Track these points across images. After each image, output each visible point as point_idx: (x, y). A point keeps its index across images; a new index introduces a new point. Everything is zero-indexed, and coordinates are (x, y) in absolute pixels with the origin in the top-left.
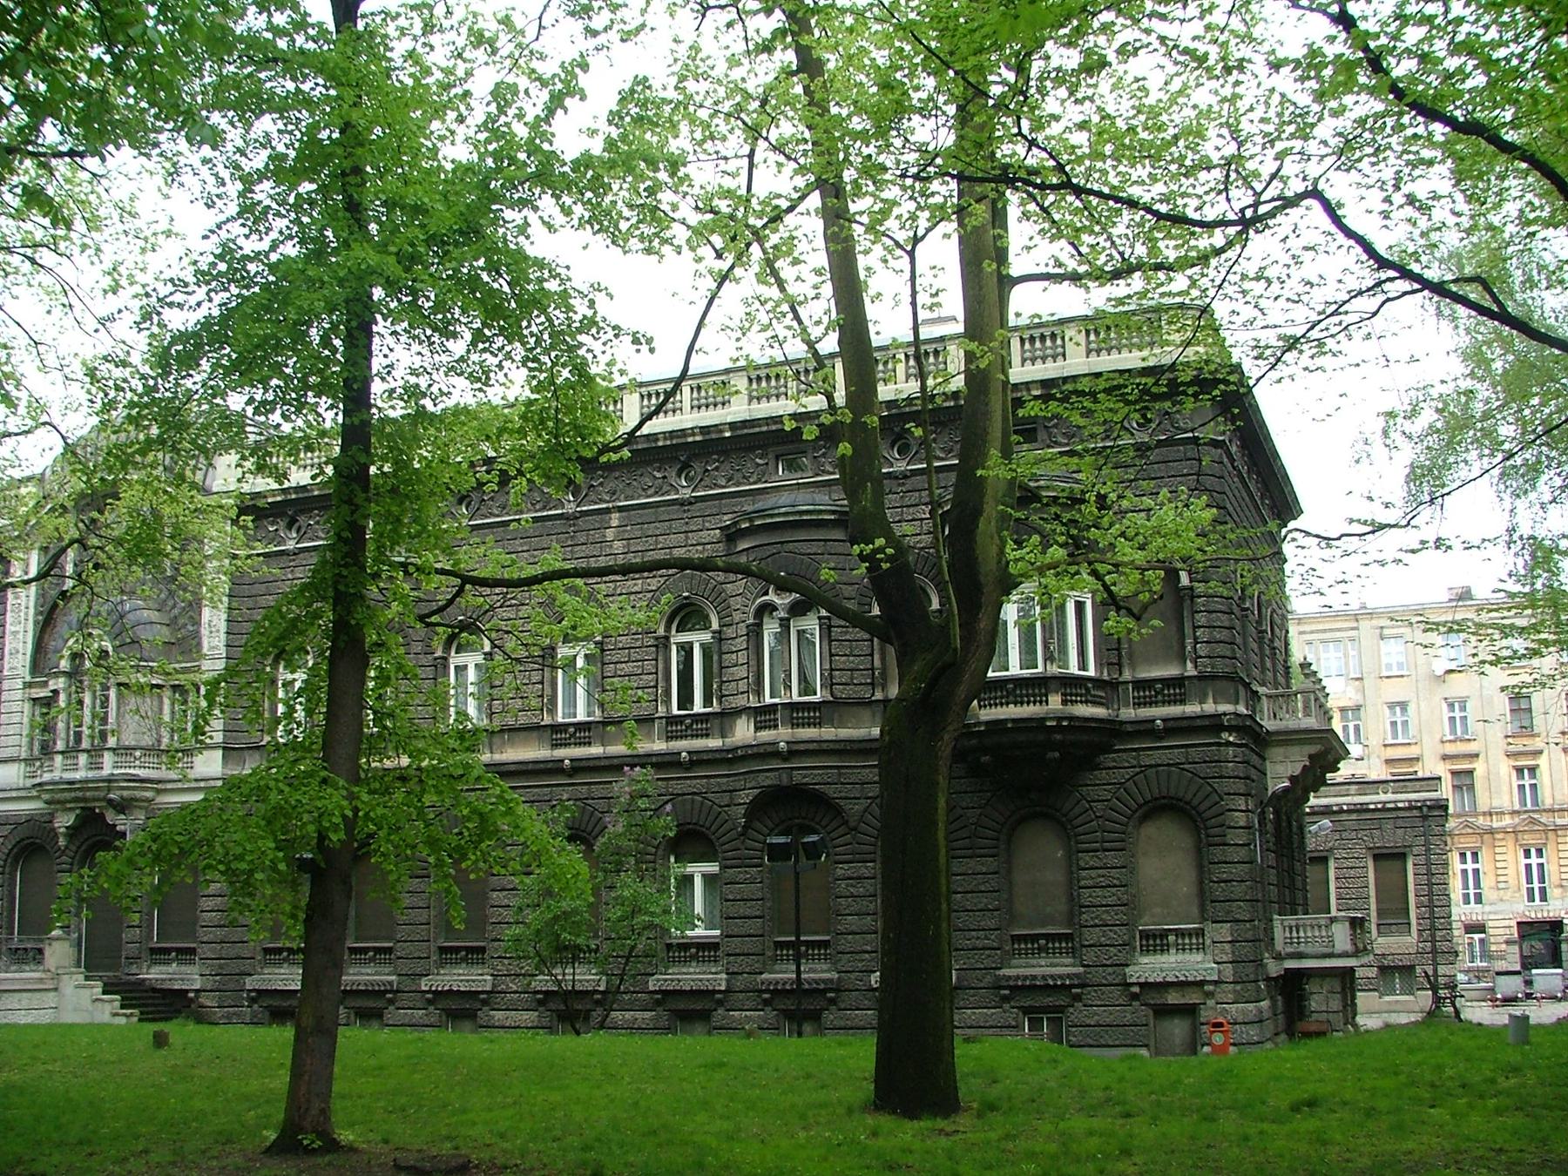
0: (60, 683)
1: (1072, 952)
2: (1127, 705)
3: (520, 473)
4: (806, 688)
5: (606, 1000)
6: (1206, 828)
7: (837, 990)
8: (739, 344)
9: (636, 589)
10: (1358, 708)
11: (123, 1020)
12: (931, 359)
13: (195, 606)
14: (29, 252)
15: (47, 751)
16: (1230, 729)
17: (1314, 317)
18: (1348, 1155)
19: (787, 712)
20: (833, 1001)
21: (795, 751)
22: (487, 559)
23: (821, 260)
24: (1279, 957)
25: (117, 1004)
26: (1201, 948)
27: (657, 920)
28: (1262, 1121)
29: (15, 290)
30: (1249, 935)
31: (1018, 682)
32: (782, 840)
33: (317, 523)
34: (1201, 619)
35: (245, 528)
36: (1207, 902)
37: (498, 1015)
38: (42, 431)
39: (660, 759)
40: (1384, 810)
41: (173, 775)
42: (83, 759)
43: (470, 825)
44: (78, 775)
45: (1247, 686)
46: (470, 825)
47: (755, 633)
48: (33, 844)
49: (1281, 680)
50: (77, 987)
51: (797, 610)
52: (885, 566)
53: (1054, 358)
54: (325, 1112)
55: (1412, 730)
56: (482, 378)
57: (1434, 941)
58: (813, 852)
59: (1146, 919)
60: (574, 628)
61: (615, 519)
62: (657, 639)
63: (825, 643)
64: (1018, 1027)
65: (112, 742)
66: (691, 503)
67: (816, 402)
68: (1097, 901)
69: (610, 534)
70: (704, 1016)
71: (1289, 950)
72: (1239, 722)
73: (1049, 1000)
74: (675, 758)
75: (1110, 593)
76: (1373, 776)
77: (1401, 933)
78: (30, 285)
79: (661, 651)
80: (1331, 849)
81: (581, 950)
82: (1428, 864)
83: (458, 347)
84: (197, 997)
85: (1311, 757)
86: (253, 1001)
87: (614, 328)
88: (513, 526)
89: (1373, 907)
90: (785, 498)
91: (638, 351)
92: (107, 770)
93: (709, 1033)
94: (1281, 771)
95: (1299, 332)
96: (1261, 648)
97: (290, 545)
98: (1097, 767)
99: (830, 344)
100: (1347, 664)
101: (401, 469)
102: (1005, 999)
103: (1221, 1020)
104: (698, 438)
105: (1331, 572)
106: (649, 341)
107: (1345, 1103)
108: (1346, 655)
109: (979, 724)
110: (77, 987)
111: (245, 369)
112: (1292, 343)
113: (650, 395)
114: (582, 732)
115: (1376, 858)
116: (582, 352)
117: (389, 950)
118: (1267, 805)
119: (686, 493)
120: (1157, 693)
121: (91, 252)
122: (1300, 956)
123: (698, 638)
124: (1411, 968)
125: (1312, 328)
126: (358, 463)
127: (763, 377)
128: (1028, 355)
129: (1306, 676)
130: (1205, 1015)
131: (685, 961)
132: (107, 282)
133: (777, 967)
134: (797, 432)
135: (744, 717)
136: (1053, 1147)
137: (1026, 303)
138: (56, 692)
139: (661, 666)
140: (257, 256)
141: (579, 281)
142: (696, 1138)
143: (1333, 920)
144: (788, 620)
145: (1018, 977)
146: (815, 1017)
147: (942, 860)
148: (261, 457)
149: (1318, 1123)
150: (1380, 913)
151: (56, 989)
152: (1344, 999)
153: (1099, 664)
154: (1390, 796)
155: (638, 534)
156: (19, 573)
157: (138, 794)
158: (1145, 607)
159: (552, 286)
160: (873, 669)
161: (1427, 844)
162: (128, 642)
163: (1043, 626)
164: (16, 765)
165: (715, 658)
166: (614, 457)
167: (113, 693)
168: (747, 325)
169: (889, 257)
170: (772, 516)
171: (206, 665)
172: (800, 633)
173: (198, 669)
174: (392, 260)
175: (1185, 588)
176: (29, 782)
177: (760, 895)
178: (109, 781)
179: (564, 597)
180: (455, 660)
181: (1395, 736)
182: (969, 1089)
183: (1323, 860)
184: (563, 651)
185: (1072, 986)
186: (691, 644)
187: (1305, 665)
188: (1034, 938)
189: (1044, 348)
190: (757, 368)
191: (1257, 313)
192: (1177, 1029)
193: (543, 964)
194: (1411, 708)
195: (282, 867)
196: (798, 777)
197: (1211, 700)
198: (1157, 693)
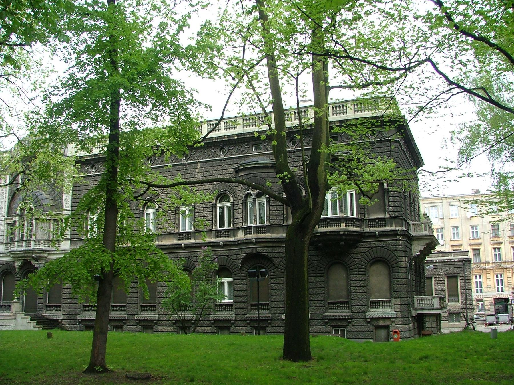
0: (17, 218)
2: (366, 227)
3: (168, 150)
4: (262, 221)
5: (196, 323)
6: (392, 267)
8: (240, 108)
10: (442, 228)
11: (37, 329)
12: (303, 114)
13: (61, 193)
15: (12, 241)
20: (270, 324)
21: (258, 242)
22: (157, 178)
24: (416, 310)
25: (35, 324)
26: (390, 306)
27: (212, 297)
30: (406, 302)
34: (391, 199)
35: (77, 168)
36: (392, 292)
37: (160, 328)
39: (213, 244)
40: (448, 262)
41: (54, 249)
42: (24, 243)
43: (151, 265)
44: (22, 249)
46: (151, 265)
47: (245, 203)
49: (417, 219)
51: (259, 195)
52: (287, 181)
53: (343, 113)
55: (460, 236)
56: (155, 119)
57: (466, 305)
59: (372, 297)
60: (185, 201)
61: (199, 165)
63: (268, 207)
64: (330, 332)
66: (224, 160)
67: (265, 127)
69: (197, 170)
70: (227, 328)
71: (419, 307)
73: (340, 324)
74: (218, 244)
76: (447, 251)
77: (456, 302)
78: (7, 88)
80: (433, 275)
81: (187, 306)
83: (148, 109)
84: (61, 321)
85: (427, 244)
86: (80, 323)
87: (199, 103)
88: (166, 167)
89: (447, 293)
90: (255, 159)
93: (229, 334)
94: (417, 249)
95: (424, 105)
97: (92, 174)
98: (357, 247)
99: (270, 108)
100: (439, 214)
101: (129, 149)
102: (326, 323)
104: (226, 139)
105: (433, 184)
106: (210, 107)
107: (437, 357)
108: (438, 212)
109: (318, 233)
111: (78, 116)
112: (421, 109)
113: (210, 125)
114: (188, 235)
115: (448, 277)
116: (188, 111)
117: (124, 306)
119: (222, 157)
121: (27, 77)
122: (423, 309)
123: (226, 205)
127: (248, 119)
128: (335, 112)
129: (425, 218)
130: (392, 328)
131: (222, 310)
132: (32, 87)
133: (252, 312)
134: (259, 137)
137: (334, 95)
138: (15, 221)
139: (214, 214)
140: (81, 79)
141: (188, 87)
143: (433, 298)
144: (256, 199)
145: (330, 316)
146: (264, 328)
147: (306, 277)
148: (83, 145)
151: (15, 319)
152: (437, 323)
153: (357, 214)
154: (452, 257)
155: (207, 170)
157: (42, 255)
158: (373, 195)
159: (179, 89)
160: (283, 215)
161: (464, 273)
162: (39, 205)
163: (339, 201)
166: (199, 145)
168: (243, 102)
169: (289, 80)
172: (260, 203)
173: (62, 214)
174: (126, 80)
175: (386, 189)
177: (246, 289)
178: (33, 251)
179: (182, 191)
180: (146, 211)
181: (454, 238)
182: (314, 352)
184: (182, 209)
185: (348, 319)
186: (224, 207)
188: (336, 303)
189: (340, 110)
191: (410, 99)
192: (383, 333)
193: (175, 311)
194: (460, 229)
195: (90, 278)
196: (259, 250)
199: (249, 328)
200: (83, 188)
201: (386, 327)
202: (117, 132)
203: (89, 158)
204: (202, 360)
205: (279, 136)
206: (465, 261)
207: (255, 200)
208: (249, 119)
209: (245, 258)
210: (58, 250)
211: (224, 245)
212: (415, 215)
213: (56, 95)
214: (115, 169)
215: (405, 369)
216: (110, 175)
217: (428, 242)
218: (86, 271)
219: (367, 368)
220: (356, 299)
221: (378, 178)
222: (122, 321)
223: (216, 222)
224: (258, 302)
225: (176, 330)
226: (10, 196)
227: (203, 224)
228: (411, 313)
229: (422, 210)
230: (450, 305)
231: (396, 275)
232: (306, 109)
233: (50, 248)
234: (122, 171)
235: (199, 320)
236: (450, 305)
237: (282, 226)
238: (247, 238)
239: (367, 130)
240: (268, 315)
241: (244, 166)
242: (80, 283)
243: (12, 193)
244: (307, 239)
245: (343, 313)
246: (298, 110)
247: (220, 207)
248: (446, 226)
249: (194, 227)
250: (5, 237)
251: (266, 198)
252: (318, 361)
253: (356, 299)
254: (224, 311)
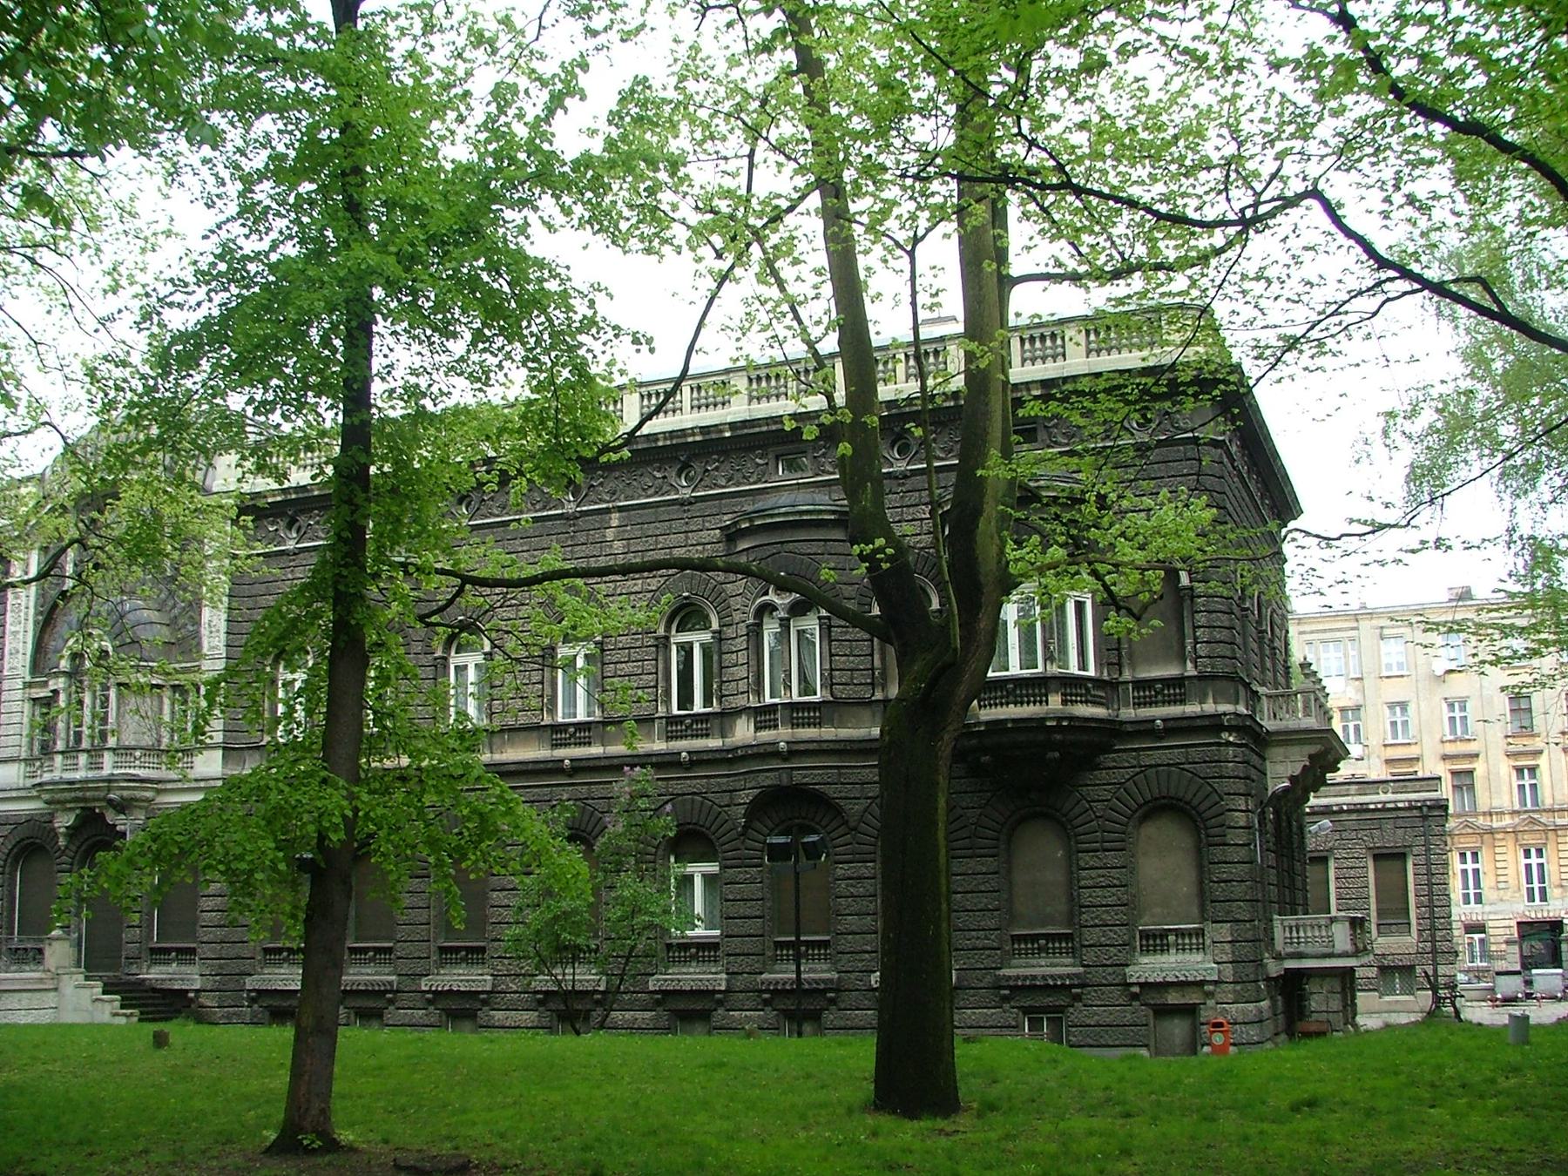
0: (60, 683)
1: (1072, 952)
2: (1127, 705)
3: (520, 473)
4: (806, 688)
5: (606, 1000)
6: (1206, 828)
7: (837, 990)
8: (739, 344)
9: (636, 589)
10: (1358, 708)
11: (123, 1020)
13: (195, 606)
14: (29, 252)
15: (47, 751)
16: (1230, 729)
17: (1314, 317)
19: (787, 712)
20: (833, 1001)
21: (795, 751)
22: (487, 559)
23: (821, 260)
24: (1279, 957)
25: (117, 1004)
26: (1201, 948)
27: (657, 920)
28: (1262, 1121)
29: (15, 290)
30: (1249, 935)
31: (1018, 682)
32: (782, 840)
33: (317, 523)
34: (1201, 619)
35: (245, 528)
36: (1207, 902)
37: (498, 1015)
38: (42, 431)
39: (660, 759)
40: (1384, 810)
41: (173, 775)
42: (83, 759)
43: (470, 825)
44: (78, 775)
45: (1247, 686)
46: (470, 825)
47: (755, 633)
48: (33, 844)
49: (1281, 680)
50: (77, 987)
51: (797, 610)
52: (885, 566)
53: (1054, 358)
54: (325, 1112)
55: (1412, 730)
56: (482, 378)
57: (1434, 941)
58: (813, 852)
59: (1146, 919)
60: (574, 628)
61: (615, 519)
62: (657, 639)
63: (825, 643)
64: (1018, 1027)
65: (112, 742)
66: (691, 503)
67: (816, 402)
68: (1097, 901)
69: (610, 534)
70: (704, 1016)
71: (1289, 950)
72: (1239, 722)
73: (1049, 1000)
74: (675, 758)
75: (1110, 593)
76: (1373, 776)
77: (1401, 933)
78: (30, 285)
79: (661, 651)
80: (1331, 849)
81: (581, 950)
82: (1428, 864)
83: (458, 347)
84: (197, 997)
85: (1311, 757)
86: (253, 1001)
87: (614, 328)
88: (513, 526)
89: (1373, 907)
90: (785, 498)
91: (638, 351)
92: (107, 770)
93: (709, 1033)
94: (1281, 771)
95: (1299, 332)
96: (1261, 648)
97: (290, 545)
98: (1097, 767)
99: (830, 344)
100: (1347, 664)
101: (401, 469)
102: (1005, 999)
103: (1221, 1020)
104: (698, 438)
105: (1331, 572)
106: (649, 341)
108: (1346, 655)
109: (979, 724)
110: (77, 987)
111: (245, 369)
112: (1292, 343)
113: (650, 395)
114: (582, 732)
115: (1376, 858)
116: (582, 352)
117: (389, 950)
118: (1267, 805)
119: (686, 493)
120: (1157, 693)
121: (91, 252)
122: (1300, 956)
123: (698, 638)
124: (1411, 968)
125: (1312, 328)
126: (358, 463)
127: (763, 377)
128: (1028, 355)
129: (1306, 676)
130: (1205, 1015)
131: (685, 961)
132: (107, 282)
133: (777, 967)
134: (797, 432)
135: (744, 717)
136: (1053, 1147)
137: (1026, 303)
138: (56, 692)
139: (661, 666)
140: (257, 256)
141: (579, 281)
142: (696, 1138)
143: (1333, 920)
144: (788, 620)
145: (1018, 977)
146: (815, 1017)
147: (942, 860)
148: (261, 457)
150: (1380, 913)
151: (56, 989)
152: (1344, 999)
153: (1099, 664)
154: (1390, 796)
155: (638, 534)
156: (19, 573)
157: (138, 794)
158: (1145, 607)
159: (552, 286)
160: (873, 669)
161: (1427, 844)
162: (128, 642)
163: (1043, 626)
164: (16, 765)
165: (715, 658)
167: (113, 693)
168: (747, 325)
169: (889, 257)
170: (772, 516)
171: (206, 665)
172: (800, 633)
173: (198, 669)
174: (392, 260)
175: (1185, 588)
176: (29, 782)
177: (760, 895)
178: (109, 781)
179: (564, 597)
180: (455, 660)
181: (1395, 736)
182: (969, 1089)
183: (1323, 860)
184: (563, 651)
185: (1072, 986)
186: (691, 644)
187: (1305, 665)
188: (1034, 938)
189: (1044, 348)
190: (757, 368)
191: (1257, 313)
192: (1177, 1029)
193: (543, 964)
194: (1411, 708)
195: (282, 867)
196: (798, 777)
197: (1211, 700)
198: (1157, 693)
239: (1126, 410)
249: (491, 715)
250: (25, 741)
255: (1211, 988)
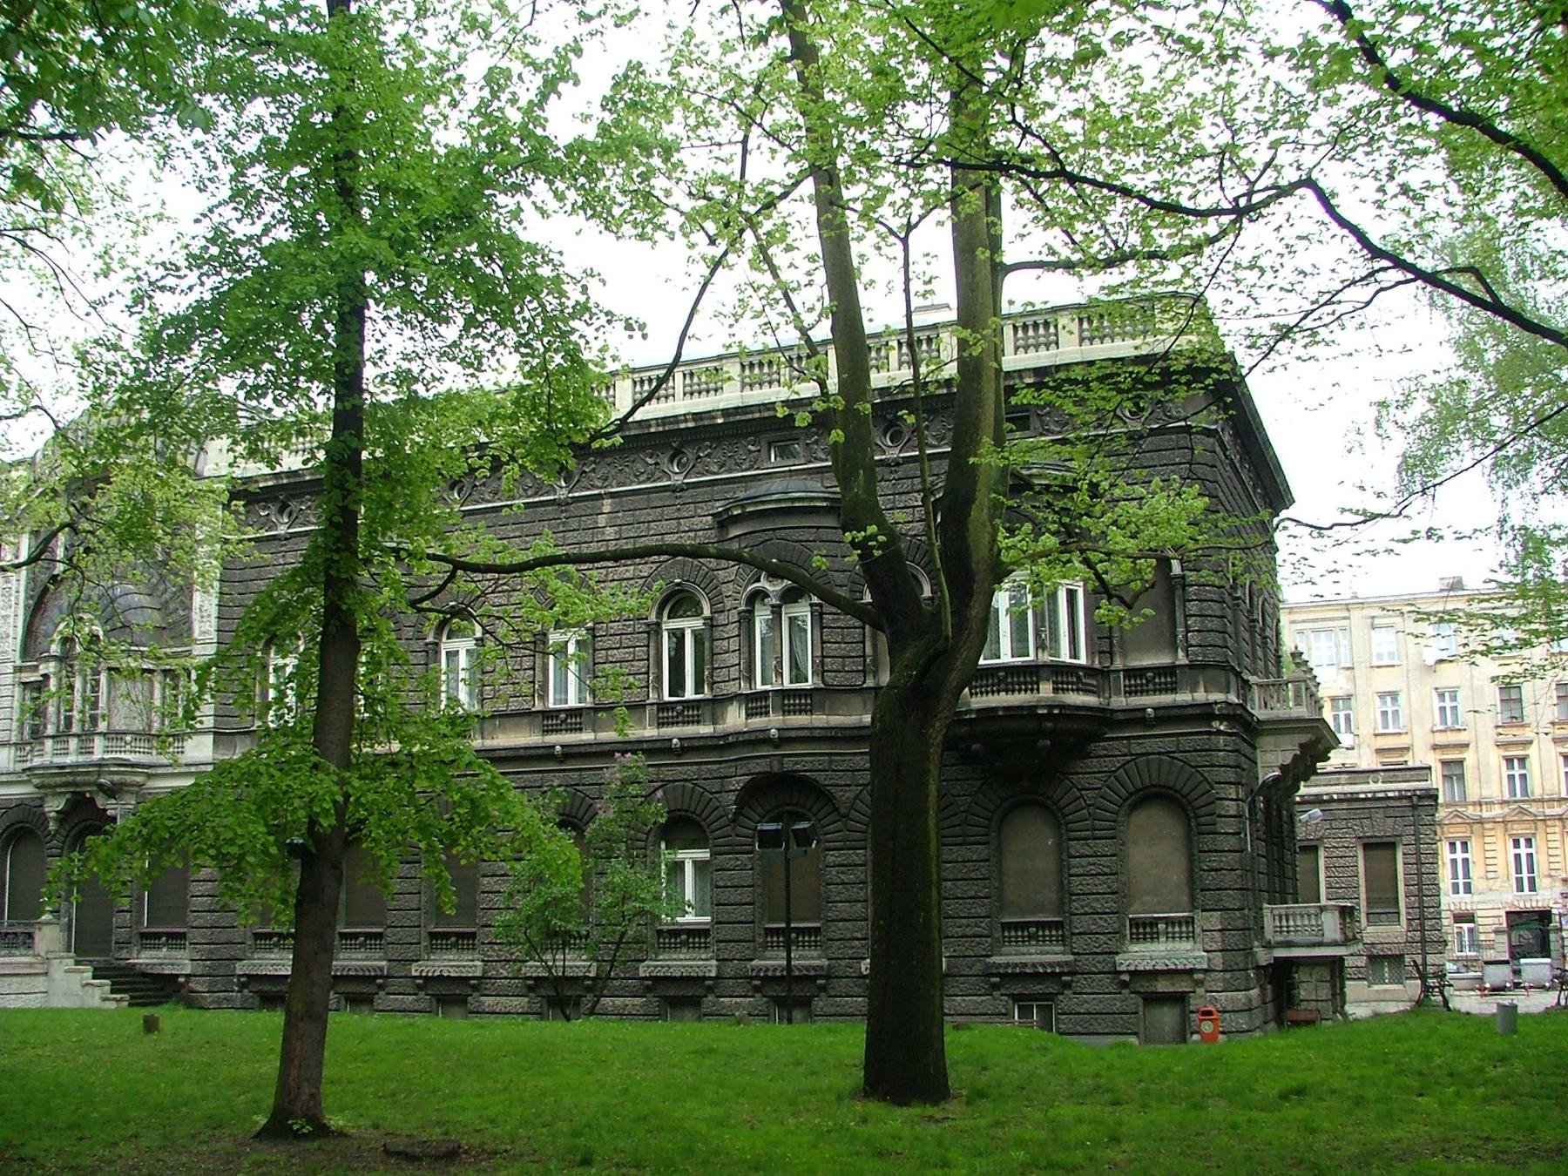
0: (50, 667)
2: (1118, 694)
3: (513, 459)
4: (798, 676)
5: (597, 986)
6: (1197, 817)
8: (732, 331)
10: (1349, 698)
11: (113, 1005)
13: (186, 591)
15: (37, 735)
18: (1336, 1143)
20: (823, 988)
21: (786, 738)
22: (478, 544)
24: (1268, 946)
25: (108, 988)
26: (1191, 936)
27: (647, 907)
30: (1239, 924)
34: (1193, 607)
35: (236, 513)
36: (1197, 890)
37: (489, 1001)
38: (33, 414)
39: (651, 745)
40: (1366, 799)
41: (163, 760)
42: (73, 743)
43: (461, 811)
44: (69, 760)
46: (461, 811)
47: (747, 619)
49: (1272, 669)
51: (789, 597)
52: (877, 553)
53: (1047, 346)
55: (1403, 720)
56: (474, 364)
57: (1423, 930)
59: (1136, 907)
60: (565, 614)
61: (607, 505)
63: (817, 634)
64: (1007, 1014)
66: (683, 490)
67: (809, 389)
69: (602, 521)
70: (694, 1002)
71: (1279, 938)
73: (1039, 988)
76: (1364, 766)
77: (1390, 922)
78: (21, 268)
80: (1320, 839)
81: (571, 936)
83: (450, 332)
84: (187, 982)
85: (1302, 746)
86: (243, 986)
87: (607, 314)
88: (505, 511)
89: (1363, 896)
90: (777, 485)
93: (699, 1019)
94: (1272, 760)
95: (1292, 321)
97: (282, 530)
98: (1088, 756)
99: (822, 331)
100: (1338, 654)
101: (393, 454)
102: (995, 986)
104: (691, 425)
105: (1322, 562)
106: (642, 327)
107: (1333, 1092)
108: (1337, 646)
109: (970, 711)
111: (237, 354)
112: (1285, 333)
113: (642, 382)
114: (573, 718)
115: (1366, 847)
116: (574, 338)
117: (380, 936)
119: (678, 480)
121: (82, 235)
122: (1289, 944)
123: (690, 625)
127: (756, 364)
128: (1021, 342)
129: (1298, 665)
130: (1195, 1003)
131: (676, 948)
132: (98, 265)
133: (768, 954)
134: (790, 419)
137: (1019, 292)
138: (46, 677)
139: (652, 653)
140: (248, 241)
141: (572, 267)
143: (1322, 909)
144: (780, 607)
145: (1008, 965)
146: (805, 1003)
147: (933, 846)
148: (253, 443)
149: (1307, 1111)
151: (46, 974)
152: (1333, 987)
153: (1090, 654)
154: (1380, 786)
155: (631, 520)
157: (129, 779)
158: (1137, 596)
159: (545, 271)
160: (864, 656)
161: (1416, 834)
162: (119, 626)
163: (1035, 615)
165: (707, 644)
166: (606, 443)
167: (103, 678)
168: (740, 311)
169: (882, 244)
171: (197, 650)
172: (792, 620)
173: (189, 654)
174: (385, 244)
175: (1177, 577)
177: (750, 882)
178: (100, 766)
179: (555, 583)
180: (446, 645)
181: (1386, 726)
182: (958, 1076)
184: (555, 637)
185: (1062, 974)
186: (682, 631)
188: (1024, 926)
189: (1037, 336)
190: (750, 354)
191: (1250, 302)
192: (1167, 1017)
193: (534, 950)
194: (1402, 698)
196: (789, 764)
199: (759, 1001)
200: (253, 573)
201: (1178, 999)
202: (357, 402)
203: (270, 483)
204: (615, 1101)
205: (850, 414)
206: (1420, 797)
207: (777, 611)
208: (761, 364)
209: (746, 787)
210: (176, 763)
211: (682, 748)
212: (1265, 655)
213: (172, 290)
214: (350, 516)
215: (1234, 1126)
216: (337, 534)
217: (1304, 738)
218: (263, 829)
219: (1120, 1124)
220: (1086, 914)
221: (1153, 544)
222: (371, 979)
223: (659, 679)
224: (788, 924)
225: (536, 1007)
226: (32, 597)
227: (620, 685)
228: (1253, 955)
229: (1289, 642)
230: (1372, 933)
231: (1207, 842)
232: (933, 334)
233: (154, 758)
234: (373, 521)
235: (608, 977)
236: (1372, 933)
237: (861, 691)
238: (752, 727)
240: (817, 962)
241: (743, 507)
242: (243, 864)
243: (38, 591)
244: (937, 731)
245: (1046, 955)
246: (910, 336)
247: (672, 633)
248: (1360, 691)
249: (593, 692)
250: (15, 725)
251: (811, 605)
252: (969, 1103)
253: (1086, 914)
254: (684, 950)
255: (1200, 976)
